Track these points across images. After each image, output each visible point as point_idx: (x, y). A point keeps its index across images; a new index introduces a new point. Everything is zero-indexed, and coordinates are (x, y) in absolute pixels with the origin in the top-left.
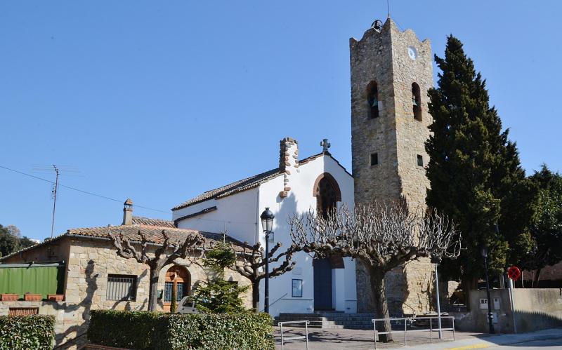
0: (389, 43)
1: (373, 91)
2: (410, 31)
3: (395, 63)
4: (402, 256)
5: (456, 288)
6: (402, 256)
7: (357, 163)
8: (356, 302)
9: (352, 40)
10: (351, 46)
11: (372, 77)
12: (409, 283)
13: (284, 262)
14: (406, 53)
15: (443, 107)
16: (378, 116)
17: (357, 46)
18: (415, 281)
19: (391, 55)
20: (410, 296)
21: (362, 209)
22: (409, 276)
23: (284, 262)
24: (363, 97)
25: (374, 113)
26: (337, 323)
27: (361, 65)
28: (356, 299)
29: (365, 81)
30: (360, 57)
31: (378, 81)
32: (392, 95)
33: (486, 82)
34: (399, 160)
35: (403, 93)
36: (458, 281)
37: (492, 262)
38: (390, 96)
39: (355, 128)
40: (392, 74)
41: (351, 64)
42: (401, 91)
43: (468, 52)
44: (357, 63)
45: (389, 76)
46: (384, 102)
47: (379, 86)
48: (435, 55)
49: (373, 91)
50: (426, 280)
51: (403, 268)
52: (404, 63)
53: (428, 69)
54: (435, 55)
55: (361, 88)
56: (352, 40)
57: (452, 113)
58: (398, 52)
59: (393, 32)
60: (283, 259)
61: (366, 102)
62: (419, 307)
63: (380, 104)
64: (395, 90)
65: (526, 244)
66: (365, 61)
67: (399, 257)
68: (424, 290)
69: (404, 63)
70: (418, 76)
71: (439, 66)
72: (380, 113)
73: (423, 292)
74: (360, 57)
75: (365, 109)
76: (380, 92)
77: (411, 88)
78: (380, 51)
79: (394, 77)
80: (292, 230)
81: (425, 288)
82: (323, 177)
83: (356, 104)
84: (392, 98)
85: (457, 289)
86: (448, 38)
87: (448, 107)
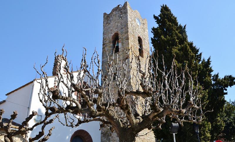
0: (126, 13)
1: (116, 38)
2: (137, 11)
3: (129, 23)
4: (156, 114)
6: (156, 114)
9: (105, 14)
10: (104, 17)
11: (115, 31)
13: (40, 132)
14: (135, 21)
15: (163, 37)
16: (119, 51)
17: (108, 16)
19: (127, 19)
23: (40, 132)
24: (110, 42)
26: (153, 41)
27: (110, 25)
29: (111, 33)
30: (109, 22)
31: (119, 32)
32: (128, 39)
33: (186, 26)
35: (134, 40)
36: (210, 135)
37: (203, 137)
38: (126, 40)
39: (104, 59)
40: (128, 28)
41: (104, 26)
42: (132, 38)
43: (175, 12)
44: (107, 25)
45: (126, 29)
46: (123, 43)
47: (119, 35)
48: (154, 15)
49: (116, 38)
52: (134, 24)
53: (146, 32)
54: (154, 15)
55: (109, 38)
56: (105, 14)
57: (168, 41)
58: (131, 18)
59: (128, 8)
60: (39, 129)
61: (111, 44)
63: (120, 45)
64: (129, 36)
65: (221, 125)
66: (111, 23)
67: (151, 117)
69: (134, 24)
70: (141, 34)
71: (156, 21)
72: (120, 50)
74: (109, 22)
75: (111, 48)
76: (120, 38)
77: (137, 39)
78: (121, 17)
79: (129, 30)
83: (105, 46)
84: (127, 41)
86: (162, 7)
87: (165, 37)
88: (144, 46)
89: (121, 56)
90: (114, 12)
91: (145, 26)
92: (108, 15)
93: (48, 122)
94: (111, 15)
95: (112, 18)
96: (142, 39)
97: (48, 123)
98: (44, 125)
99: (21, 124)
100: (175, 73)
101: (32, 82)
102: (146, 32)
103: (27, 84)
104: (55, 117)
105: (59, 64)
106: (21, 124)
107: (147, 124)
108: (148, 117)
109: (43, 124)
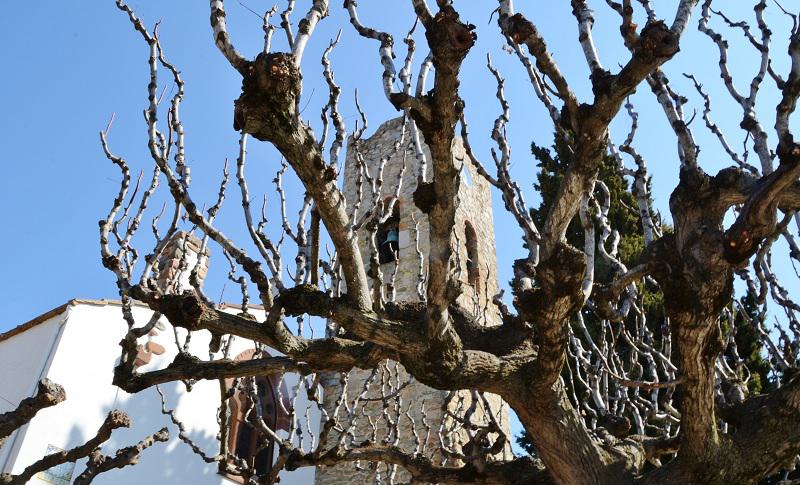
48: (533, 144)
54: (533, 144)
88: (480, 257)
89: (407, 275)
90: (387, 133)
91: (483, 194)
92: (365, 141)
93: (108, 458)
94: (376, 144)
95: (377, 151)
96: (477, 233)
97: (108, 464)
98: (86, 472)
99: (434, 16)
100: (573, 397)
101: (61, 310)
102: (487, 215)
103: (19, 327)
104: (152, 439)
105: (179, 253)
106: (434, 16)
107: (787, 445)
108: (785, 401)
109: (82, 464)
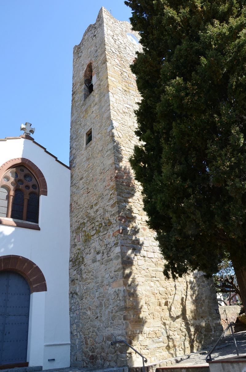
5: (239, 312)
7: (74, 151)
8: (68, 348)
12: (142, 303)
18: (153, 299)
20: (146, 329)
21: (231, 343)
22: (142, 291)
25: (90, 88)
28: (70, 343)
34: (115, 124)
50: (178, 298)
51: (129, 276)
62: (168, 348)
68: (174, 315)
73: (174, 319)
80: (79, 361)
81: (177, 310)
82: (20, 161)
85: (240, 314)
